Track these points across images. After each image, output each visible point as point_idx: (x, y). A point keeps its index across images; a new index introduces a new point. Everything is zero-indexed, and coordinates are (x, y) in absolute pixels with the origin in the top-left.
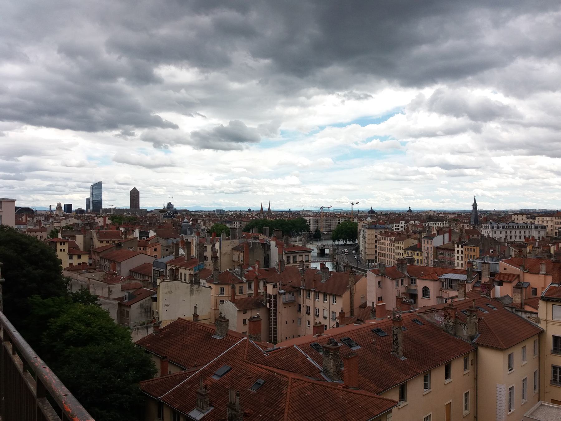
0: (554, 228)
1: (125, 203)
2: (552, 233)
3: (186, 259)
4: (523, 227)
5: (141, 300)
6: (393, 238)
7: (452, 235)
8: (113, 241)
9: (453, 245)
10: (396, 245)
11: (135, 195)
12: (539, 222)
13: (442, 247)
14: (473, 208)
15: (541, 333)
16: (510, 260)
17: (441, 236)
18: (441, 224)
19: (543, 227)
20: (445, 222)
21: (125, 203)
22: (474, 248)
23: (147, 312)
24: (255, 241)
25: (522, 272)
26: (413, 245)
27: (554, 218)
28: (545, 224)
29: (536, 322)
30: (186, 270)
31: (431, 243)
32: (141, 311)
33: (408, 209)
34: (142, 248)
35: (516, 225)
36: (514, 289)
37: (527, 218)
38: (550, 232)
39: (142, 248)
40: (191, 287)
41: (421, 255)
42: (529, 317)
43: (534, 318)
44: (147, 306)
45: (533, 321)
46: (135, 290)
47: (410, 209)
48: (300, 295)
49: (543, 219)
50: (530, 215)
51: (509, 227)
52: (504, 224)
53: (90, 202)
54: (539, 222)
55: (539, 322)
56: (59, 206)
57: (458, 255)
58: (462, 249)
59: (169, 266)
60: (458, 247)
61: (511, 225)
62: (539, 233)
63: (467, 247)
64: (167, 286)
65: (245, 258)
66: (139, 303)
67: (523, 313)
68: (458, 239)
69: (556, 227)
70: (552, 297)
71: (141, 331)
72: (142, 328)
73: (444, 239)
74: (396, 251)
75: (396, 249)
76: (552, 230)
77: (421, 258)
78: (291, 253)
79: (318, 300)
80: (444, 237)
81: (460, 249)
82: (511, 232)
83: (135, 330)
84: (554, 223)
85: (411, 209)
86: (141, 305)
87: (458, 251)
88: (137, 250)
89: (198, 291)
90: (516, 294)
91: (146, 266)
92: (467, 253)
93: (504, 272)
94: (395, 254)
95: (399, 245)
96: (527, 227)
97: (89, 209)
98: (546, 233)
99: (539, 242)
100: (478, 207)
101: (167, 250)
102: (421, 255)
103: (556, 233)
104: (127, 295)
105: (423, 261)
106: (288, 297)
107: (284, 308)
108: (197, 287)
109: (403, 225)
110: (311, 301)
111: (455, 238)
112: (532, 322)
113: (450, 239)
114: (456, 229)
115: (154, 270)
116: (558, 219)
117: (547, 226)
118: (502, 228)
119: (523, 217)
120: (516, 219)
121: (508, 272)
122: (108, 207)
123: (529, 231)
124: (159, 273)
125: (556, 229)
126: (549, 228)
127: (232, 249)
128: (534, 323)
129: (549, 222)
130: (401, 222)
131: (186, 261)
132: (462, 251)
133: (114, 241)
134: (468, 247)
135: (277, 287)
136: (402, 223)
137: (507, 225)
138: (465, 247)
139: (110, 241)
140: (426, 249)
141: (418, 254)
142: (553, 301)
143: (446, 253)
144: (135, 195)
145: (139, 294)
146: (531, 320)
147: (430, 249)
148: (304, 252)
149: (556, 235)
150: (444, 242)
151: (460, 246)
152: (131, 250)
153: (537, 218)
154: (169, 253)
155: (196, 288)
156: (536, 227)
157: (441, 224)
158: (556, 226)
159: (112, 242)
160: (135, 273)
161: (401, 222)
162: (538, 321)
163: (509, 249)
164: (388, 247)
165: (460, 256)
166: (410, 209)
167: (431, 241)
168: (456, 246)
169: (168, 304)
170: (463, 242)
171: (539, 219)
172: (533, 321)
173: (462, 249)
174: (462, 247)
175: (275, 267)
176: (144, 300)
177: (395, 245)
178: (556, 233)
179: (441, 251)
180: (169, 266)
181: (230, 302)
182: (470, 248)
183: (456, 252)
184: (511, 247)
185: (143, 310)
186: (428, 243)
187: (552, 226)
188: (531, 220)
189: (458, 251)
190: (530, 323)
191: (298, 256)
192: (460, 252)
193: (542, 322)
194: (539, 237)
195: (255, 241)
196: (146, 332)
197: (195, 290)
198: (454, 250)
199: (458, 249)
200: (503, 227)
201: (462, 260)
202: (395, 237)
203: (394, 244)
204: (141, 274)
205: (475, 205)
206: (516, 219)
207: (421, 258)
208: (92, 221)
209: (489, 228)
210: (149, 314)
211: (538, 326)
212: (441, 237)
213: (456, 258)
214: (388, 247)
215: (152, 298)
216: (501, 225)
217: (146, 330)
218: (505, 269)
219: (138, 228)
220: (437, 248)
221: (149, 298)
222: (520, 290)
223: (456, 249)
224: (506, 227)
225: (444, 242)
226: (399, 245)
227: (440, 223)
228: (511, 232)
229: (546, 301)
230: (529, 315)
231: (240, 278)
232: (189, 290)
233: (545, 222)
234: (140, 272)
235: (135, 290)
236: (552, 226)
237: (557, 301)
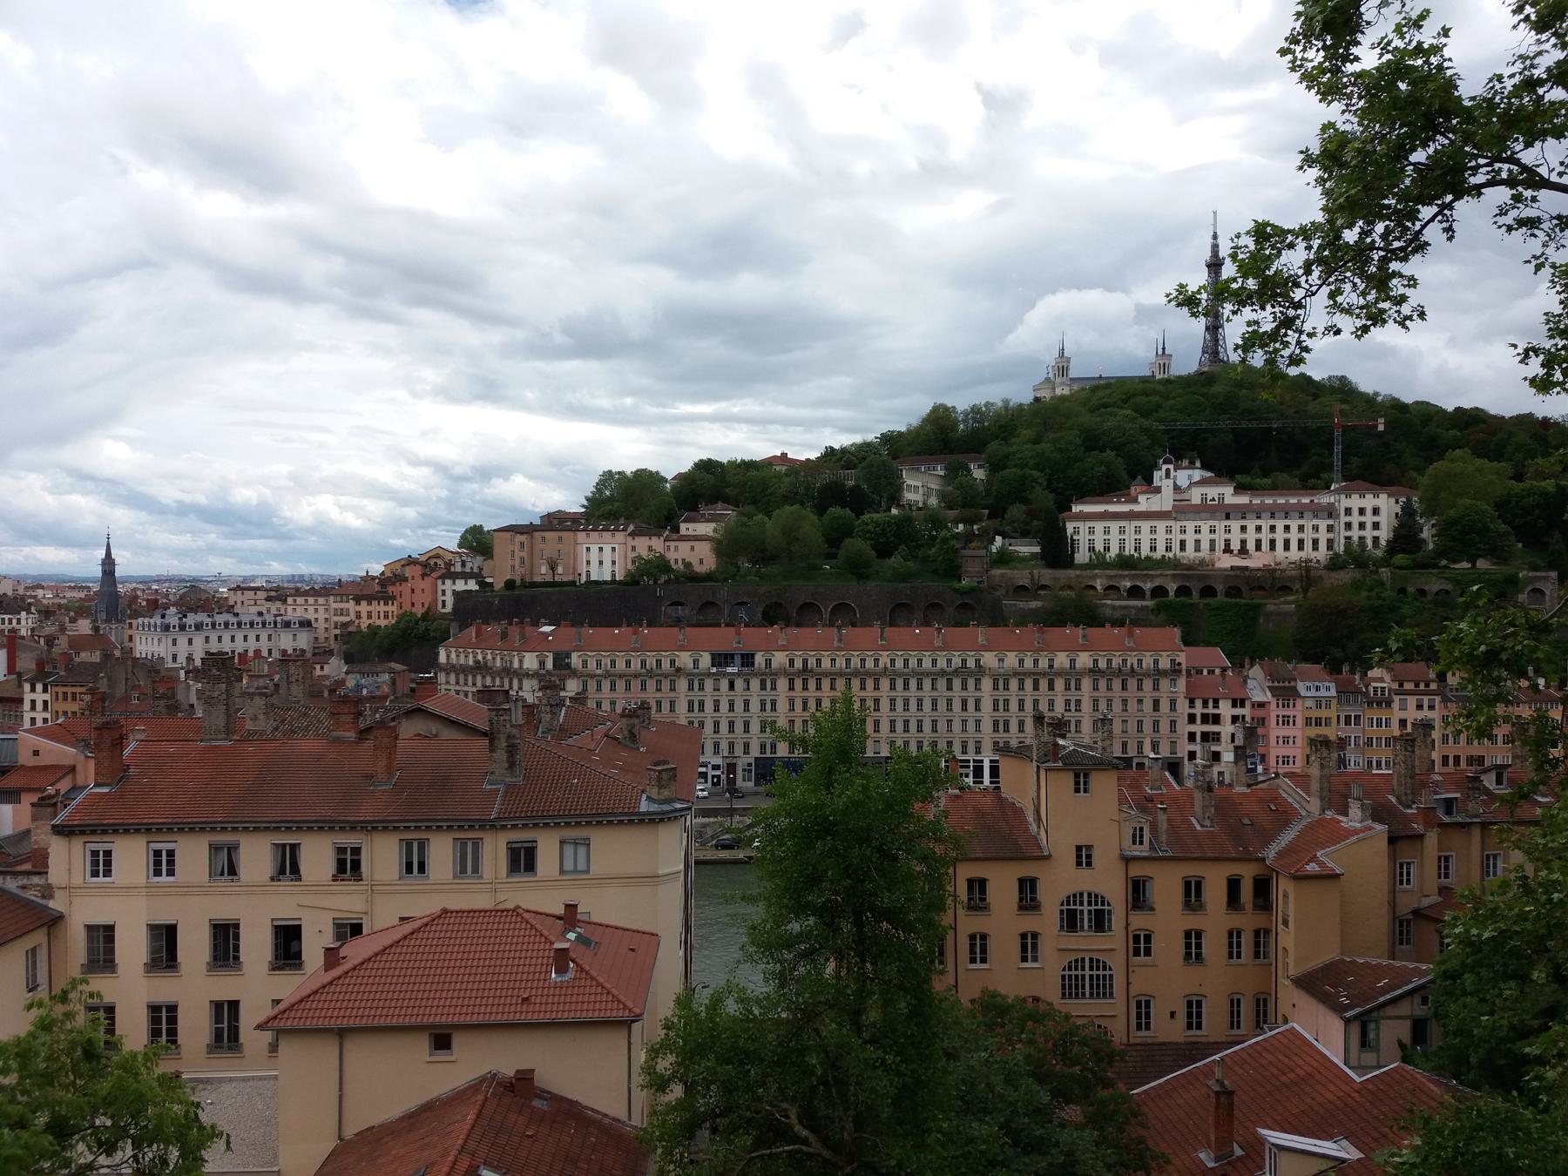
0: (333, 626)
1: (457, 581)
2: (326, 638)
4: (252, 624)
7: (18, 653)
9: (20, 686)
12: (295, 610)
14: (104, 572)
15: (54, 921)
16: (60, 725)
18: (10, 620)
19: (306, 624)
20: (23, 614)
21: (457, 581)
25: (82, 757)
27: (332, 599)
28: (311, 616)
29: (43, 897)
35: (234, 620)
36: (35, 809)
37: (269, 599)
38: (322, 634)
42: (23, 887)
43: (38, 885)
45: (36, 896)
49: (306, 600)
50: (276, 591)
51: (213, 625)
52: (202, 617)
54: (295, 610)
55: (51, 897)
57: (33, 715)
58: (47, 697)
60: (33, 690)
61: (220, 619)
63: (61, 690)
67: (8, 877)
68: (33, 666)
69: (336, 623)
70: (82, 822)
81: (40, 697)
84: (332, 613)
87: (33, 702)
90: (40, 822)
93: (32, 762)
96: (264, 624)
98: (312, 640)
99: (270, 664)
100: (117, 568)
111: (26, 663)
112: (33, 898)
114: (39, 637)
116: (341, 602)
117: (316, 619)
118: (193, 628)
119: (256, 597)
120: (239, 603)
121: (44, 760)
123: (270, 636)
125: (336, 628)
126: (321, 625)
128: (38, 900)
132: (45, 703)
134: (65, 689)
137: (209, 620)
142: (83, 833)
146: (30, 895)
151: (39, 687)
153: (290, 600)
156: (287, 625)
157: (10, 620)
158: (336, 619)
162: (48, 891)
163: (188, 686)
168: (27, 687)
170: (49, 674)
171: (295, 601)
172: (36, 896)
173: (47, 697)
174: (45, 690)
182: (69, 690)
183: (27, 705)
184: (191, 683)
187: (326, 620)
188: (278, 604)
189: (33, 702)
190: (28, 902)
192: (39, 706)
193: (57, 894)
194: (295, 650)
198: (20, 701)
199: (33, 696)
200: (199, 627)
205: (108, 563)
206: (239, 603)
209: (156, 630)
211: (47, 907)
216: (191, 619)
218: (36, 753)
222: (49, 810)
223: (28, 697)
224: (207, 625)
229: (68, 835)
230: (25, 881)
233: (311, 609)
236: (326, 620)
237: (93, 832)
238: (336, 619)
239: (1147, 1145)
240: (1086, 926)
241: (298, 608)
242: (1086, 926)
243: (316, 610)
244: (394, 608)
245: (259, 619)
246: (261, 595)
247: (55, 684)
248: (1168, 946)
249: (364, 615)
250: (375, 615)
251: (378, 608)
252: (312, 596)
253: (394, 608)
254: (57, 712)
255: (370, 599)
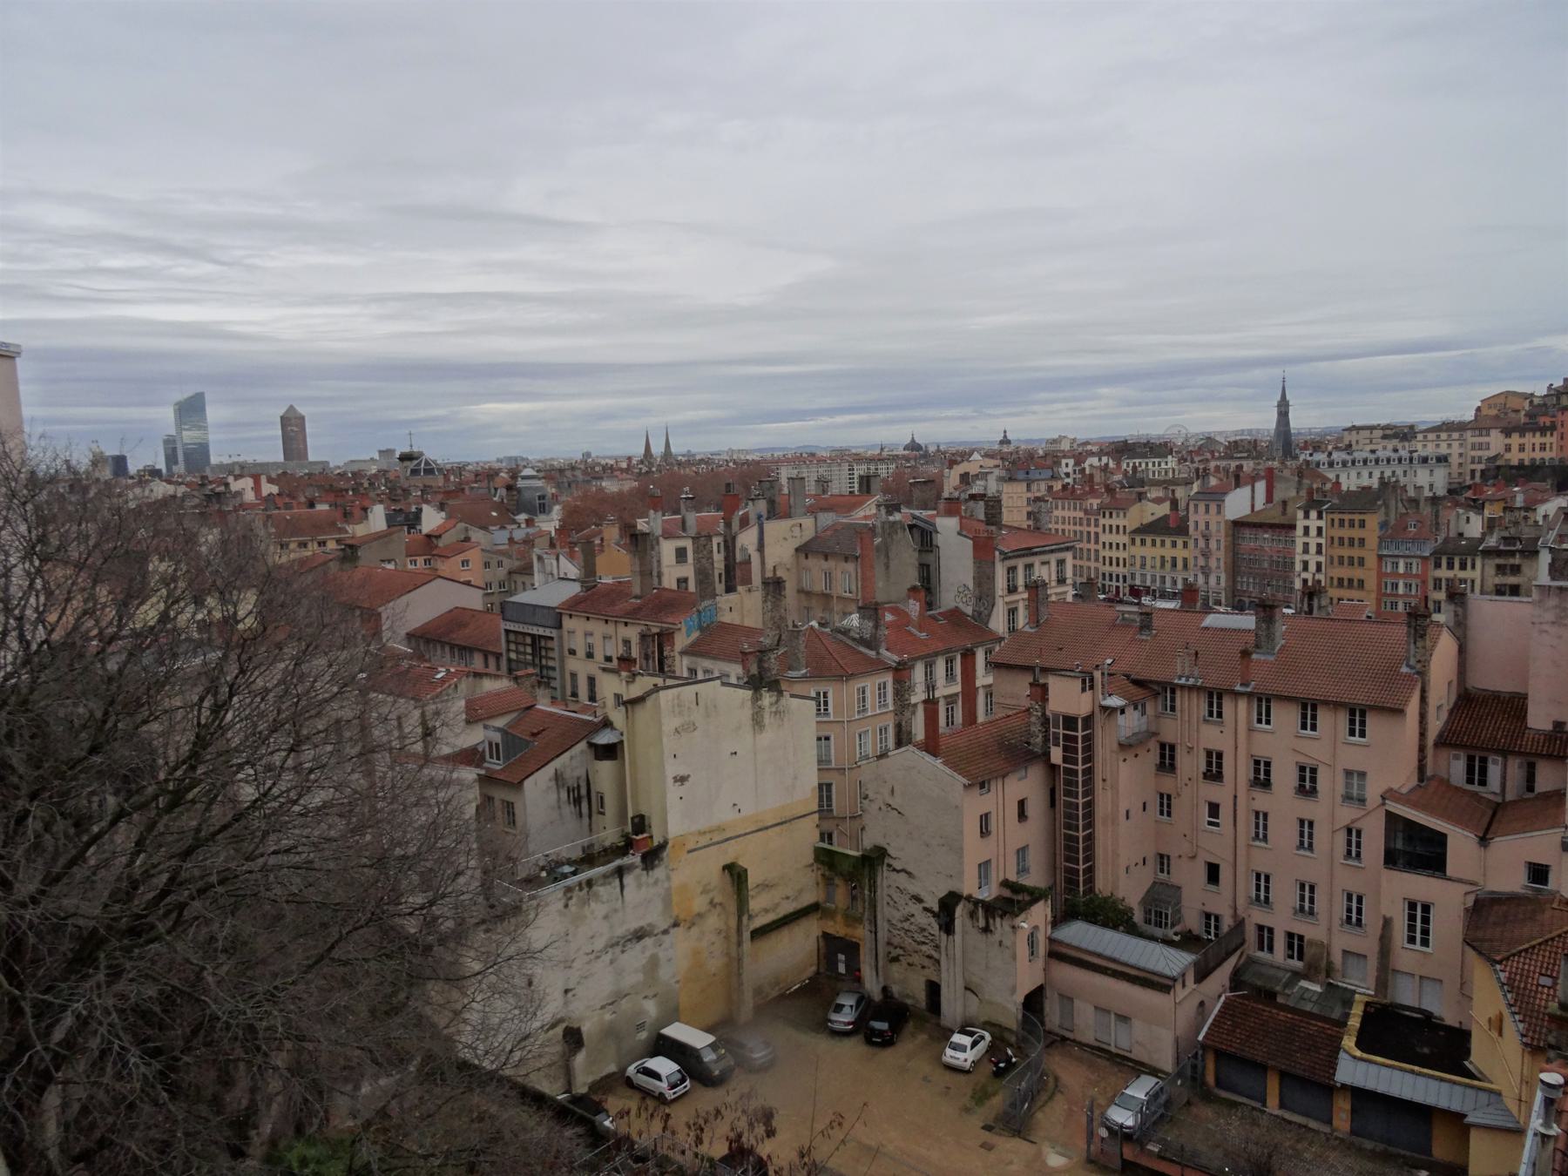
0: (1469, 460)
2: (1460, 474)
3: (637, 590)
4: (1388, 461)
5: (558, 756)
6: (1095, 503)
8: (319, 544)
10: (1106, 521)
11: (292, 427)
13: (1250, 520)
17: (1246, 491)
19: (1442, 459)
22: (1362, 517)
23: (577, 801)
24: (891, 518)
26: (1154, 518)
27: (1469, 433)
28: (1443, 450)
30: (591, 621)
31: (1219, 512)
32: (559, 799)
33: (908, 441)
34: (420, 560)
37: (1385, 437)
39: (420, 560)
40: (756, 698)
41: (1185, 545)
44: (578, 778)
46: (514, 715)
47: (913, 440)
48: (1173, 709)
49: (1438, 437)
53: (174, 450)
56: (97, 461)
58: (1322, 523)
59: (571, 616)
60: (1307, 516)
62: (1431, 475)
63: (1337, 517)
64: (679, 706)
65: (863, 579)
66: (549, 771)
69: (1473, 458)
71: (601, 889)
72: (605, 876)
73: (1253, 498)
74: (1103, 538)
75: (1104, 531)
76: (1460, 464)
77: (1185, 553)
78: (1019, 556)
79: (1264, 726)
80: (1253, 491)
81: (1314, 523)
82: (1371, 474)
83: (581, 889)
84: (1469, 447)
85: (1010, 437)
86: (558, 777)
88: (405, 565)
89: (776, 713)
91: (457, 618)
92: (1338, 533)
94: (1100, 547)
95: (1114, 522)
96: (1400, 460)
97: (175, 469)
101: (500, 564)
102: (1185, 545)
103: (1473, 472)
104: (499, 741)
105: (1191, 563)
106: (1130, 723)
107: (1121, 763)
108: (774, 699)
109: (1070, 470)
110: (1229, 729)
113: (1269, 498)
115: (507, 631)
122: (226, 460)
123: (1405, 472)
124: (529, 640)
125: (1473, 462)
127: (797, 550)
129: (1455, 445)
130: (1064, 462)
131: (636, 597)
133: (322, 543)
135: (1092, 687)
136: (1067, 465)
138: (1331, 516)
139: (310, 545)
140: (1202, 526)
141: (1174, 544)
143: (1266, 536)
144: (292, 427)
145: (538, 733)
147: (1213, 527)
148: (1052, 551)
149: (1473, 477)
150: (1253, 506)
151: (1313, 514)
152: (391, 566)
154: (505, 572)
155: (771, 704)
156: (1425, 460)
158: (1473, 453)
159: (316, 545)
160: (428, 641)
161: (1064, 462)
164: (1078, 528)
165: (1313, 541)
166: (913, 440)
167: (1219, 507)
168: (1300, 514)
169: (682, 772)
170: (1322, 503)
173: (1322, 523)
174: (1320, 517)
175: (961, 606)
176: (567, 755)
177: (1102, 521)
178: (1473, 472)
179: (1247, 533)
180: (571, 616)
181: (917, 752)
182: (1347, 517)
183: (1299, 531)
185: (564, 795)
186: (1207, 511)
187: (1461, 455)
191: (1037, 565)
192: (1313, 532)
195: (891, 518)
196: (618, 889)
197: (767, 709)
198: (1293, 527)
199: (1307, 523)
201: (1319, 552)
202: (1099, 501)
203: (1096, 520)
204: (452, 647)
207: (1185, 553)
208: (222, 488)
210: (585, 805)
212: (1244, 492)
213: (1299, 548)
214: (1078, 528)
215: (591, 745)
217: (617, 882)
219: (381, 502)
220: (1238, 525)
221: (582, 745)
223: (1300, 524)
225: (1253, 506)
226: (1114, 522)
227: (1157, 460)
228: (1371, 474)
231: (872, 654)
232: (748, 712)
233: (1444, 445)
234: (446, 640)
235: (514, 715)
236: (1461, 455)
238: (1473, 453)
239: (969, 898)
240: (1080, 721)
241: (1429, 444)
242: (1080, 721)
243: (1449, 446)
244: (1554, 439)
245: (1372, 457)
246: (1378, 433)
247: (1331, 510)
248: (1283, 832)
249: (1515, 448)
250: (1528, 447)
251: (1533, 440)
252: (1446, 431)
253: (1554, 439)
254: (1332, 538)
255: (1522, 430)
